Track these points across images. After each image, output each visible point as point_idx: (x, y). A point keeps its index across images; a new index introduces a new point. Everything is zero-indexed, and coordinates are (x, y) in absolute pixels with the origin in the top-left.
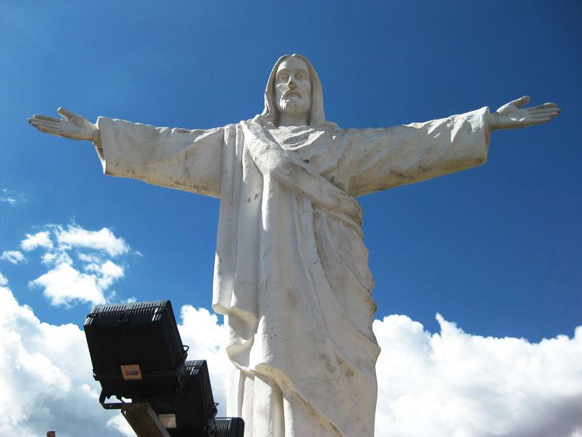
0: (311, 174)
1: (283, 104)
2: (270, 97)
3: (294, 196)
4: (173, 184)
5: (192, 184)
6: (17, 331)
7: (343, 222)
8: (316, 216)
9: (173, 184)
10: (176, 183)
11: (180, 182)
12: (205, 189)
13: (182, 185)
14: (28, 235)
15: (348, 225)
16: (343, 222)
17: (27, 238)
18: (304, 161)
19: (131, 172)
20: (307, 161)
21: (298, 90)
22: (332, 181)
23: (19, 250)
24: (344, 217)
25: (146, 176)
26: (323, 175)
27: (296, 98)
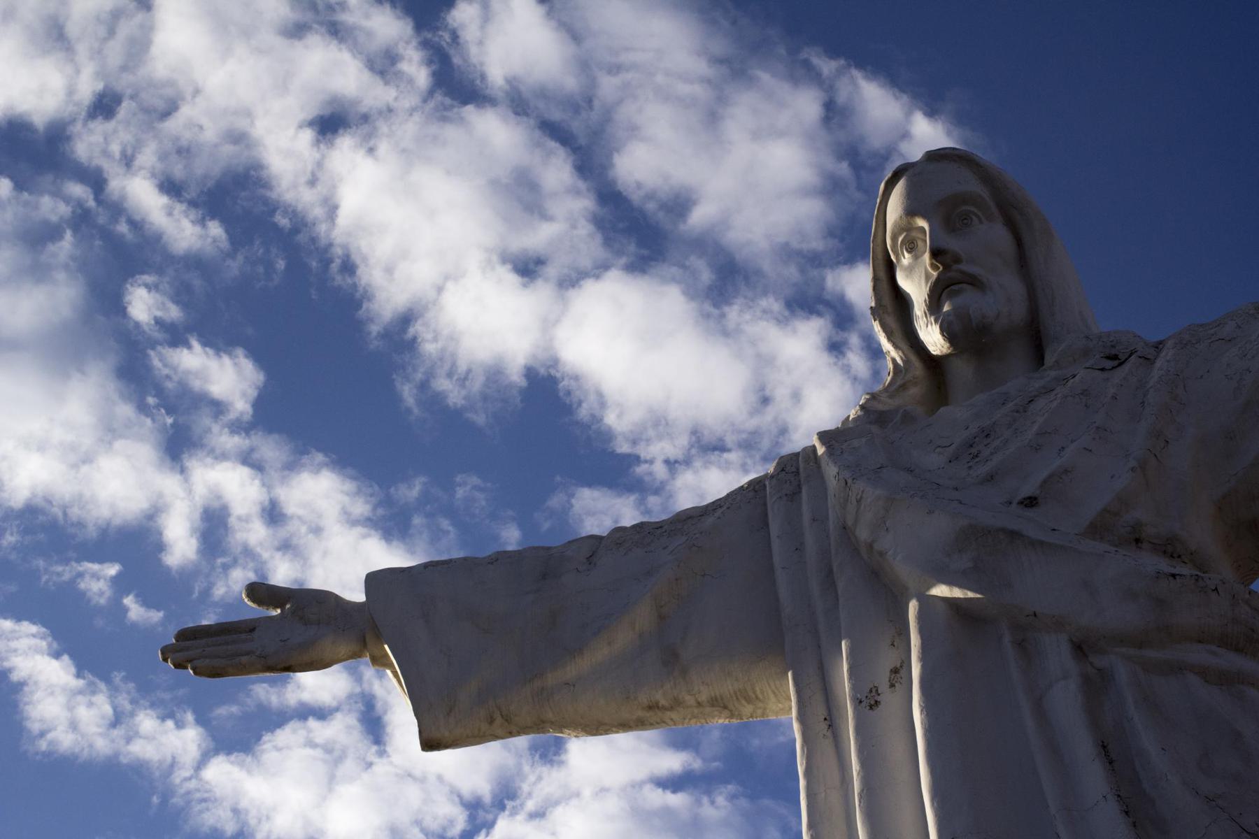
0: (1042, 543)
1: (933, 338)
2: (891, 321)
3: (1007, 639)
4: (640, 713)
5: (703, 698)
6: (188, 372)
7: (1203, 673)
8: (1096, 687)
9: (640, 713)
10: (650, 708)
11: (663, 702)
12: (749, 700)
13: (671, 708)
14: (195, 344)
15: (1225, 680)
16: (1203, 673)
17: (189, 347)
18: (1021, 503)
19: (499, 720)
20: (1031, 502)
21: (963, 267)
22: (1138, 541)
23: (290, 719)
24: (1198, 655)
25: (550, 716)
26: (1096, 530)
27: (969, 297)
